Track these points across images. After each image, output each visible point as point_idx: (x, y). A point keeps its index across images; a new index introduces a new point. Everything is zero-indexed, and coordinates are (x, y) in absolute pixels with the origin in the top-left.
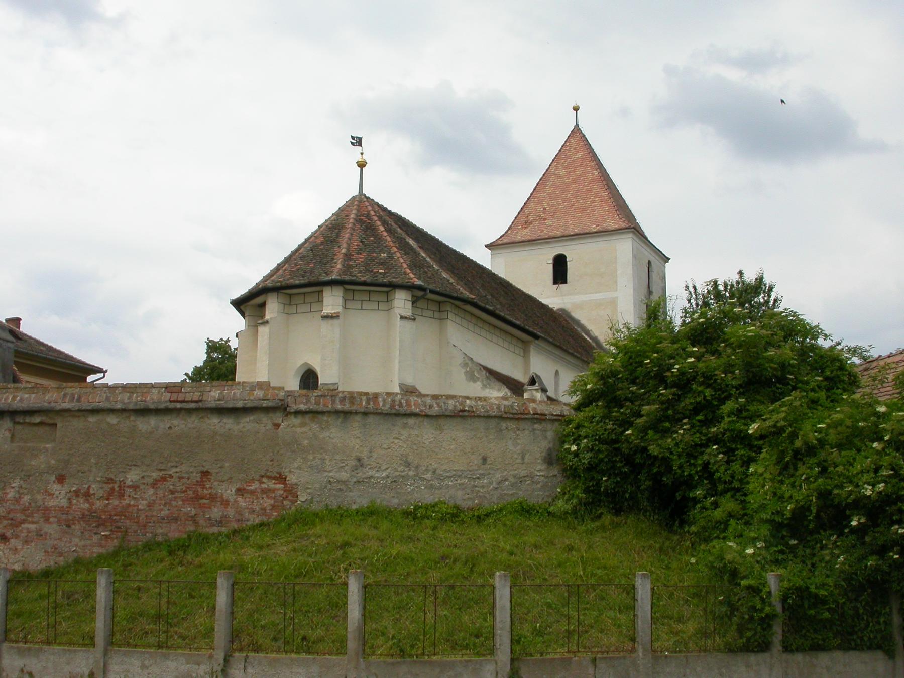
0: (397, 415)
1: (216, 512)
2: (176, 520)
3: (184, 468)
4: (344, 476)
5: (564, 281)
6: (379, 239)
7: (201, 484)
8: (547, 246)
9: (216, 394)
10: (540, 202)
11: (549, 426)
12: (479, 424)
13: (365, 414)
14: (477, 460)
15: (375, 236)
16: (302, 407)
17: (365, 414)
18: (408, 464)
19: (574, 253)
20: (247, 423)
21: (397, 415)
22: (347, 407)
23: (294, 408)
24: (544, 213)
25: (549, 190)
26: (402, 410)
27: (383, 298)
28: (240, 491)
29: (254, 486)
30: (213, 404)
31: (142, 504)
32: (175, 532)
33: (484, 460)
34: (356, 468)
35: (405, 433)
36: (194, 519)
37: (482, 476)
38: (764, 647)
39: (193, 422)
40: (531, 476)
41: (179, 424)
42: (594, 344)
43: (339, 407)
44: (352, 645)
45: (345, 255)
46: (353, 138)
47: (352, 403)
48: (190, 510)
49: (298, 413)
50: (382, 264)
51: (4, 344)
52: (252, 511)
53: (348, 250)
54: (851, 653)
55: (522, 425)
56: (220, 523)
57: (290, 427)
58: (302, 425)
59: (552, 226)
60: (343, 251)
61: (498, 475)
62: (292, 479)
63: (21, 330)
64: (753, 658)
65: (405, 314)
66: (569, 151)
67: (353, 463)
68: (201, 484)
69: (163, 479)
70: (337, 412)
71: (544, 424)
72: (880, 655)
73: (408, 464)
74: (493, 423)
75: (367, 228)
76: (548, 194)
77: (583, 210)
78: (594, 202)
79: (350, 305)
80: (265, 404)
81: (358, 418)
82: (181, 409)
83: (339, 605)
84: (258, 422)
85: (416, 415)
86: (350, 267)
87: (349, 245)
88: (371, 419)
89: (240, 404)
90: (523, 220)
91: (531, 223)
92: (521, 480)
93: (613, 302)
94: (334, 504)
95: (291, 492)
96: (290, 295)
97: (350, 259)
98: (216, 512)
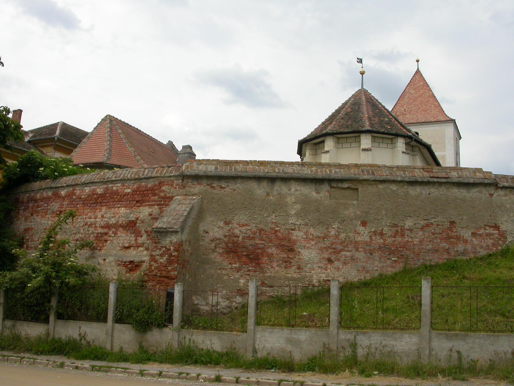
3: (439, 219)
7: (450, 229)
10: (402, 106)
20: (474, 192)
24: (405, 111)
29: (482, 231)
31: (416, 241)
36: (447, 251)
41: (435, 192)
46: (358, 59)
49: (504, 188)
52: (482, 247)
58: (506, 195)
62: (503, 227)
69: (427, 225)
82: (434, 183)
84: (481, 192)
95: (503, 235)
96: (338, 138)
98: (460, 247)
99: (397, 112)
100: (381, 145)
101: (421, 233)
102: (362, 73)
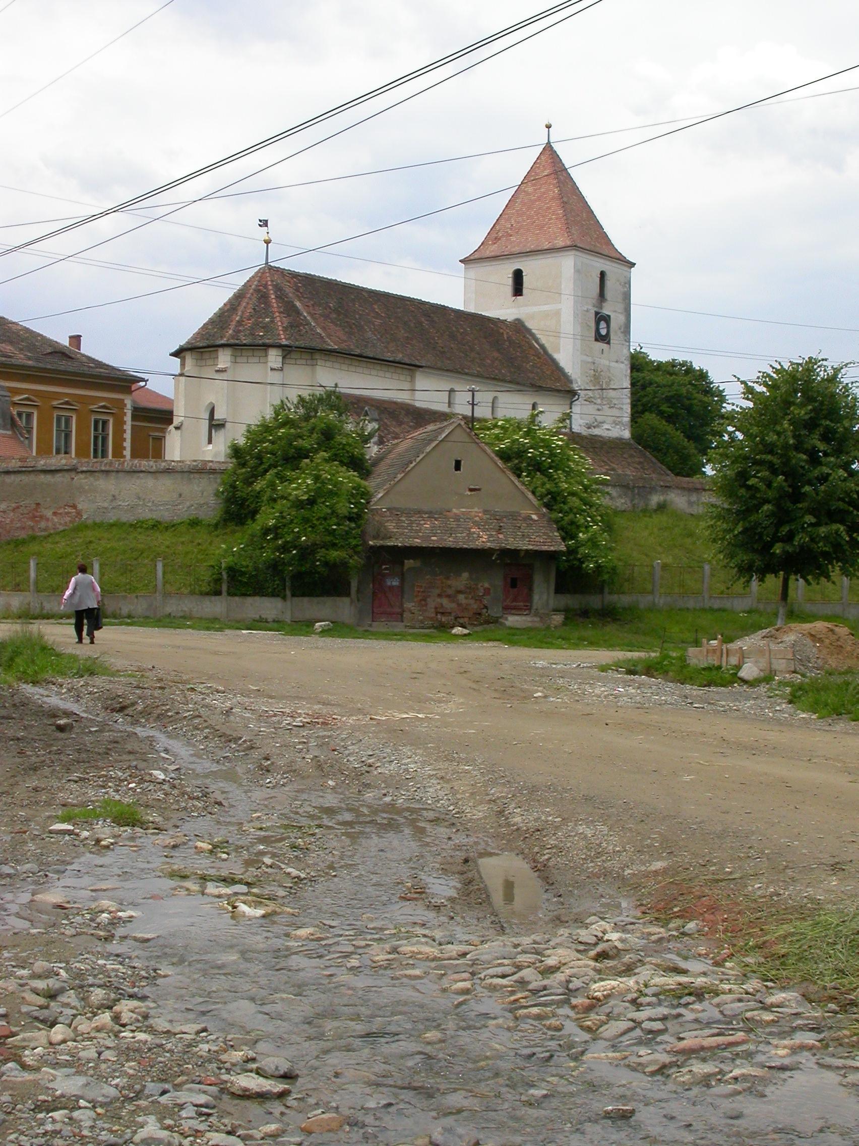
0: (134, 472)
1: (43, 524)
2: (24, 528)
3: (27, 502)
4: (106, 505)
5: (521, 295)
6: (268, 304)
7: (36, 510)
8: (507, 261)
9: (42, 462)
10: (509, 220)
11: (219, 476)
12: (179, 476)
13: (117, 472)
14: (175, 496)
15: (265, 303)
16: (84, 469)
17: (117, 472)
18: (139, 498)
19: (531, 269)
20: (58, 478)
21: (134, 472)
22: (107, 468)
23: (81, 469)
24: (511, 229)
25: (518, 206)
26: (136, 469)
27: (262, 353)
28: (55, 514)
29: (61, 511)
30: (39, 468)
31: (8, 521)
32: (22, 535)
33: (180, 495)
34: (112, 501)
35: (138, 481)
36: (32, 528)
37: (179, 504)
38: (218, 593)
39: (32, 477)
40: (207, 504)
41: (25, 478)
42: (541, 351)
43: (103, 468)
44: (32, 588)
45: (238, 321)
46: (260, 221)
47: (110, 466)
48: (31, 523)
49: (82, 472)
50: (263, 328)
51: (3, 399)
52: (61, 524)
53: (241, 317)
54: (264, 598)
55: (203, 476)
56: (45, 530)
57: (80, 479)
58: (86, 478)
59: (515, 243)
60: (237, 319)
61: (188, 504)
62: (80, 507)
63: (83, 351)
64: (213, 598)
65: (275, 366)
66: (539, 168)
67: (111, 498)
68: (36, 510)
69: (18, 507)
70: (102, 471)
71: (215, 475)
72: (279, 599)
73: (139, 498)
74: (186, 475)
75: (262, 296)
76: (517, 211)
77: (541, 227)
78: (550, 219)
79: (238, 360)
80: (66, 468)
81: (114, 474)
82: (25, 471)
83: (27, 571)
84: (63, 477)
85: (142, 472)
86: (240, 331)
87: (243, 312)
88: (120, 475)
89: (53, 468)
90: (495, 235)
91: (499, 239)
92: (201, 506)
93: (558, 313)
94: (98, 520)
95: (79, 514)
96: (202, 352)
97: (241, 325)
98: (43, 524)
99: (499, 231)
100: (251, 360)
101: (12, 514)
102: (267, 242)
